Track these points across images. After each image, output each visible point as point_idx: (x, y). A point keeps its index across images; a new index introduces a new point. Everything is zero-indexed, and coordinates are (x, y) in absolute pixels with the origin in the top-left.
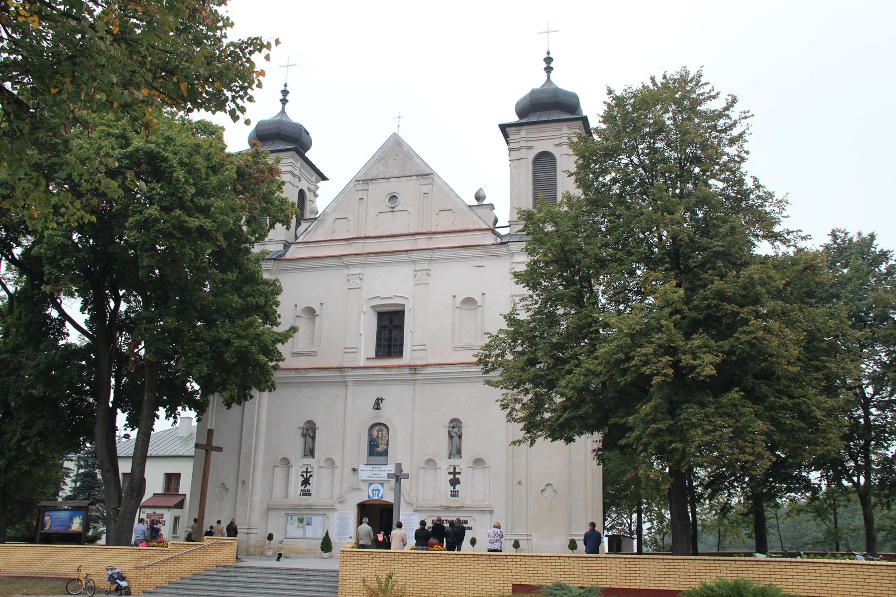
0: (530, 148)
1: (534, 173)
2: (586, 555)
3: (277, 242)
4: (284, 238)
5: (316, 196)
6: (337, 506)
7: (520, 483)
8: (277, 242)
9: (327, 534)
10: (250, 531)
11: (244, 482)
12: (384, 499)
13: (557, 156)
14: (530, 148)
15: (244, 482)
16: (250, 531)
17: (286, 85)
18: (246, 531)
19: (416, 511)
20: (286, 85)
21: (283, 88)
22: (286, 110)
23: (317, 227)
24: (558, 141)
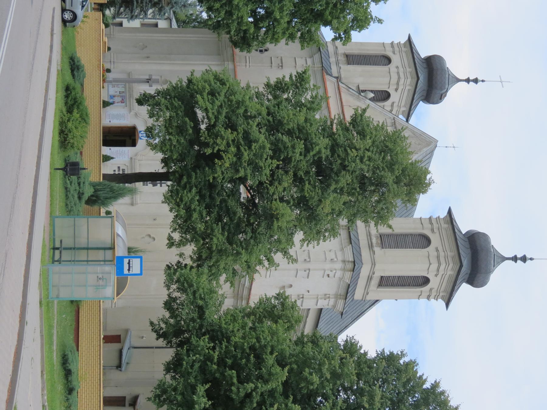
0: (396, 90)
1: (411, 235)
2: (102, 337)
3: (339, 72)
4: (342, 76)
5: (428, 298)
6: (132, 113)
7: (154, 220)
8: (339, 72)
9: (112, 158)
10: (112, 63)
11: (148, 57)
12: (139, 140)
13: (428, 249)
14: (433, 230)
15: (148, 57)
16: (112, 63)
17: (531, 259)
18: (112, 60)
19: (131, 158)
20: (531, 259)
21: (528, 256)
22: (507, 261)
23: (353, 95)
24: (440, 249)
